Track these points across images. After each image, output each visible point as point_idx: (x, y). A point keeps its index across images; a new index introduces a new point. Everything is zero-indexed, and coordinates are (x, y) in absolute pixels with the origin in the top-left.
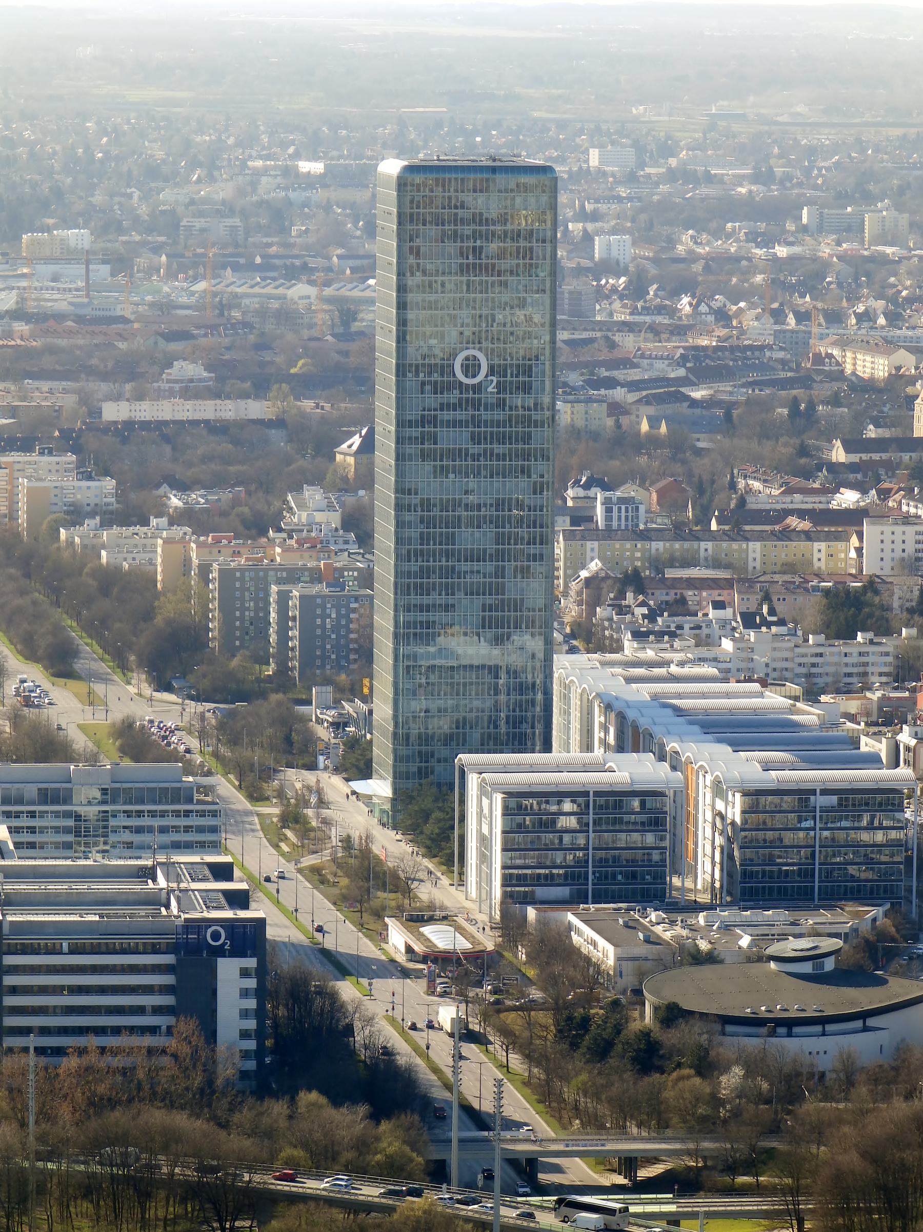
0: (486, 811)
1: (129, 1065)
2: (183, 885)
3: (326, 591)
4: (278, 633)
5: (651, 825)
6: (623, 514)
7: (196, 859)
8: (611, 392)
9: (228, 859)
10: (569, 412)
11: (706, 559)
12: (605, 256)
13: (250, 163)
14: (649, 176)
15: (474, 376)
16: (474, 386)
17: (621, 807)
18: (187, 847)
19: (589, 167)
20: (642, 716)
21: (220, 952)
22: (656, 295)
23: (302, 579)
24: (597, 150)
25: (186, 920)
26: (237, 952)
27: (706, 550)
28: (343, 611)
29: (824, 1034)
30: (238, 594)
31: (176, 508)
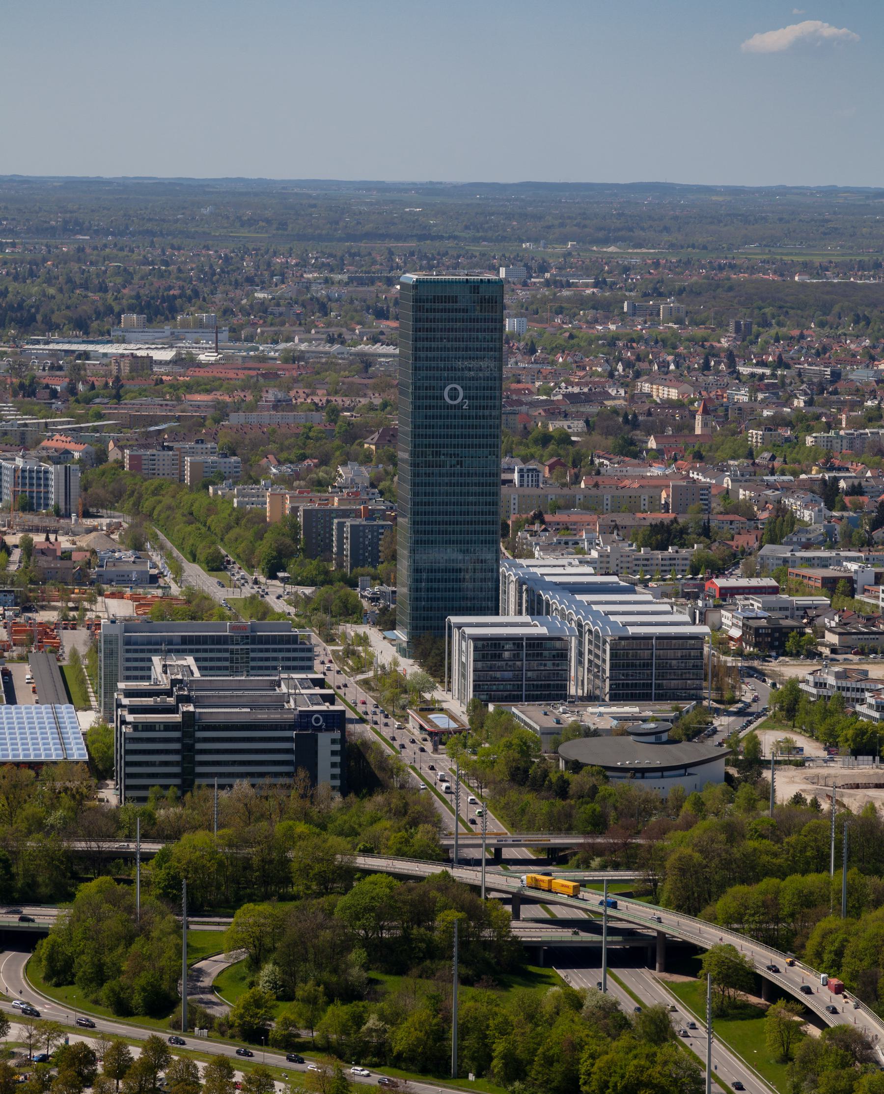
0: (464, 648)
1: (669, 794)
2: (297, 691)
3: (364, 523)
4: (337, 547)
6: (530, 478)
7: (303, 676)
11: (579, 504)
12: (511, 329)
14: (535, 283)
15: (455, 399)
16: (455, 406)
17: (541, 647)
18: (295, 669)
21: (319, 729)
25: (300, 711)
26: (329, 729)
29: (662, 777)
31: (274, 475)
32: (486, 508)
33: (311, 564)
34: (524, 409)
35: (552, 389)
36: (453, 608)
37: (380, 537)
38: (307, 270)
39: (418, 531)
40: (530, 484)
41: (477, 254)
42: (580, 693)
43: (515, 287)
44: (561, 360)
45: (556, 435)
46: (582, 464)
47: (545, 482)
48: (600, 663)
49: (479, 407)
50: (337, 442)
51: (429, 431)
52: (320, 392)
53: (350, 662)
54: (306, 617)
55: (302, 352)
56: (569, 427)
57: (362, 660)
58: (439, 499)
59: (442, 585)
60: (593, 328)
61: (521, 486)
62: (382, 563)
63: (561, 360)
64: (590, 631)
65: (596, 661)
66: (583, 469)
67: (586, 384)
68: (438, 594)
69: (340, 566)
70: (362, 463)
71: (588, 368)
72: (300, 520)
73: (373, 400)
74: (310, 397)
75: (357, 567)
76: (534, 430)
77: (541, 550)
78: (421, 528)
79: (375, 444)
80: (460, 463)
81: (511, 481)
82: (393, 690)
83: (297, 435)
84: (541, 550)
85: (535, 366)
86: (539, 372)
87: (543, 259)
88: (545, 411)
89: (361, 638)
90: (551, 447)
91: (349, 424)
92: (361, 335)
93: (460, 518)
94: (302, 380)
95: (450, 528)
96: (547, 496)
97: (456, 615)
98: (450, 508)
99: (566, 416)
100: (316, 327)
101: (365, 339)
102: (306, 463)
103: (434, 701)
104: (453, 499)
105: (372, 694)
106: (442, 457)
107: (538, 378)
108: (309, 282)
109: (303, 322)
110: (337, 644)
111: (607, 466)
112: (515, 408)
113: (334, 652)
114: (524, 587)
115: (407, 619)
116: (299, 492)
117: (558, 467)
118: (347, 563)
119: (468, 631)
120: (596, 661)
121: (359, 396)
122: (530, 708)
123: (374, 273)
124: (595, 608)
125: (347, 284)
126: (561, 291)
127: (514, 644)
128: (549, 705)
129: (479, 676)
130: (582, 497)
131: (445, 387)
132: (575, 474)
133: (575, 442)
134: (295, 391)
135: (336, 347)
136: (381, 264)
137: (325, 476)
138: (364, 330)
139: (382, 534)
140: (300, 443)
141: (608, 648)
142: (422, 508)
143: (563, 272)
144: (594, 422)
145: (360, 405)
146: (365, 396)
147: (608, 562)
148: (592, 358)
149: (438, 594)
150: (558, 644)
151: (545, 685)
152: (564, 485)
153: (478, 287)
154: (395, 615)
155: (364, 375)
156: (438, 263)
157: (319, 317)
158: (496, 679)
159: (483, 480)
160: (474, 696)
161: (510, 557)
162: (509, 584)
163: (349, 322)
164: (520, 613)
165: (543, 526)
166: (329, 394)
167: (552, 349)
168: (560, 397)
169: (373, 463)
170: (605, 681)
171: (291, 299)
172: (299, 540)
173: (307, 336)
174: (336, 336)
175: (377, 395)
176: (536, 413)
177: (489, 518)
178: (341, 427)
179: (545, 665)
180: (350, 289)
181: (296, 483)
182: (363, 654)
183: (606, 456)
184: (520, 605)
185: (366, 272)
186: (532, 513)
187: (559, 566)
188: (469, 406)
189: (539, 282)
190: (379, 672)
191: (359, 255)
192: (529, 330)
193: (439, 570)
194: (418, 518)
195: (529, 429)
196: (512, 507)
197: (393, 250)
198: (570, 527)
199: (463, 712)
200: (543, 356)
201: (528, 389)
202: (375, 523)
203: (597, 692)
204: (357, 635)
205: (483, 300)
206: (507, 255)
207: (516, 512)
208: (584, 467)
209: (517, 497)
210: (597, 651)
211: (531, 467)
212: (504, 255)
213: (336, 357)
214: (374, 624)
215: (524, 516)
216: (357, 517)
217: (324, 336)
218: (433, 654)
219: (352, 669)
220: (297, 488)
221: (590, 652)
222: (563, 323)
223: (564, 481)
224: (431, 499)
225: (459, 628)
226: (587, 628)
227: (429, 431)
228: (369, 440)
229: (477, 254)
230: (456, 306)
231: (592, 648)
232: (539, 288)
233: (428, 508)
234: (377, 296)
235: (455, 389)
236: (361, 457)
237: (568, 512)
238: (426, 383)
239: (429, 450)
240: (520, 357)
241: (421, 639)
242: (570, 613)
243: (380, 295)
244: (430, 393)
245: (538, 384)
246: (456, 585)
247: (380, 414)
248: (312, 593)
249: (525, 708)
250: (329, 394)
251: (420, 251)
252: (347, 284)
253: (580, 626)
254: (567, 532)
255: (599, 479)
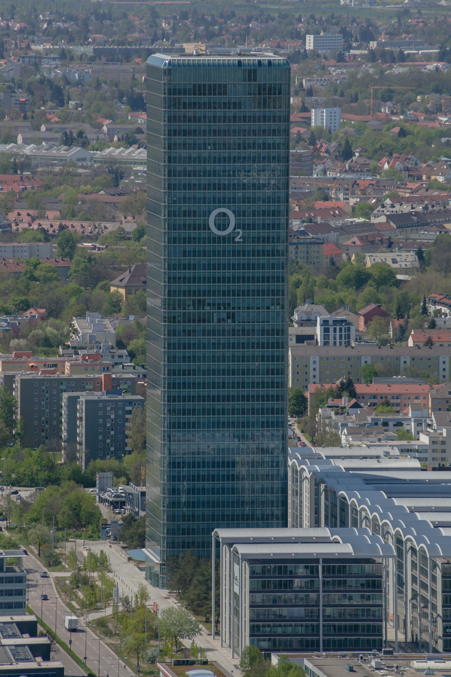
0: (237, 574)
3: (105, 397)
4: (68, 431)
5: (369, 587)
6: (338, 333)
8: (326, 235)
9: (32, 618)
10: (294, 252)
11: (405, 369)
13: (33, 47)
14: (355, 56)
15: (224, 229)
16: (224, 238)
19: (305, 50)
20: (339, 484)
22: (360, 156)
23: (87, 387)
24: (312, 36)
27: (366, 362)
28: (120, 412)
30: (36, 400)
32: (268, 378)
33: (31, 455)
34: (333, 236)
35: (372, 208)
36: (223, 516)
37: (127, 416)
38: (36, 38)
39: (174, 411)
40: (338, 341)
41: (276, 15)
42: (401, 637)
43: (327, 63)
44: (386, 166)
45: (376, 274)
46: (411, 312)
47: (359, 339)
48: (428, 596)
49: (257, 240)
50: (73, 285)
51: (189, 273)
52: (51, 214)
53: (80, 595)
54: (21, 530)
55: (27, 157)
56: (394, 261)
57: (97, 591)
58: (204, 366)
59: (208, 484)
60: (434, 120)
61: (326, 344)
62: (130, 452)
63: (386, 166)
64: (413, 550)
65: (423, 592)
66: (411, 320)
67: (421, 200)
68: (204, 497)
69: (72, 457)
70: (108, 314)
71: (424, 177)
72: (17, 394)
73: (124, 226)
74: (37, 222)
75: (95, 459)
76: (345, 265)
77: (349, 434)
78: (179, 405)
79: (126, 287)
80: (232, 316)
81: (311, 337)
82: (137, 635)
83: (17, 275)
84: (349, 434)
85: (349, 176)
86: (355, 183)
87: (368, 20)
88: (361, 238)
89: (96, 560)
90: (368, 289)
91: (90, 260)
92: (111, 133)
93: (233, 392)
94: (26, 198)
95: (219, 405)
96: (359, 358)
97: (228, 526)
98: (218, 378)
99: (390, 245)
100: (48, 121)
101: (116, 139)
102: (29, 314)
103: (196, 650)
104: (223, 365)
105: (110, 641)
106: (207, 308)
107: (353, 193)
108: (39, 57)
109: (29, 114)
110: (64, 569)
111: (446, 315)
112: (320, 236)
113: (58, 581)
114: (322, 487)
115: (161, 533)
116: (17, 356)
117: (376, 318)
118: (82, 454)
119: (243, 549)
120: (423, 592)
121: (104, 219)
122: (329, 661)
123: (130, 44)
124: (420, 516)
125: (92, 60)
126: (391, 67)
127: (306, 567)
128: (356, 656)
129: (258, 614)
130: (408, 360)
131: (210, 212)
132: (401, 326)
133: (401, 281)
134: (16, 212)
135: (76, 150)
136: (141, 32)
137: (55, 332)
138: (115, 126)
139: (130, 412)
140: (21, 286)
141: (439, 574)
142: (180, 379)
143: (396, 39)
144: (429, 253)
145: (106, 232)
146: (113, 219)
147: (444, 451)
148: (430, 162)
149: (204, 497)
150: (368, 568)
151: (350, 626)
152: (384, 342)
153: (255, 71)
154: (144, 527)
155: (113, 191)
156: (221, 29)
157: (51, 108)
158: (281, 618)
159: (264, 339)
160: (252, 642)
161: (307, 443)
162: (301, 482)
163: (93, 115)
164: (316, 523)
165: (354, 401)
166: (63, 217)
167: (376, 151)
168: (383, 219)
169: (122, 314)
170: (436, 621)
171: (13, 81)
172: (14, 422)
173: (36, 134)
174: (75, 135)
175: (130, 218)
176: (349, 242)
177: (273, 391)
178: (78, 264)
179: (350, 598)
180: (96, 67)
181: (14, 342)
182: (99, 583)
183: (445, 301)
184: (317, 511)
185: (118, 44)
186: (338, 382)
187: (372, 457)
188: (243, 238)
189: (361, 55)
190: (121, 609)
191: (110, 19)
192: (343, 125)
193: (204, 464)
194: (175, 392)
195: (338, 264)
196: (312, 373)
197: (158, 10)
198: (392, 401)
199: (236, 666)
200: (362, 161)
201: (338, 208)
202: (120, 398)
203: (425, 637)
204: (91, 555)
205: (261, 89)
206: (317, 16)
207: (317, 379)
208: (414, 316)
209: (317, 359)
210: (423, 578)
211: (339, 318)
212: (313, 17)
213: (74, 165)
214: (116, 539)
215: (327, 386)
216: (95, 389)
217: (59, 135)
218: (195, 581)
219: (83, 604)
220: (15, 349)
221: (414, 579)
222: (393, 113)
223: (385, 336)
224: (192, 365)
225: (230, 545)
226: (409, 545)
227: (189, 273)
228: (116, 281)
229: (276, 15)
230: (223, 99)
231: (417, 574)
232: (360, 65)
233: (188, 379)
234: (134, 79)
235: (224, 215)
236: (106, 306)
237: (389, 380)
238: (185, 207)
239: (189, 299)
240: (329, 163)
241: (180, 559)
242: (385, 524)
243: (137, 76)
244: (189, 220)
245: (352, 201)
246: (228, 484)
247: (134, 245)
248: (30, 496)
249: (321, 661)
250: (63, 217)
251: (195, 12)
252: (92, 60)
253: (399, 541)
254: (386, 409)
255: (434, 334)
